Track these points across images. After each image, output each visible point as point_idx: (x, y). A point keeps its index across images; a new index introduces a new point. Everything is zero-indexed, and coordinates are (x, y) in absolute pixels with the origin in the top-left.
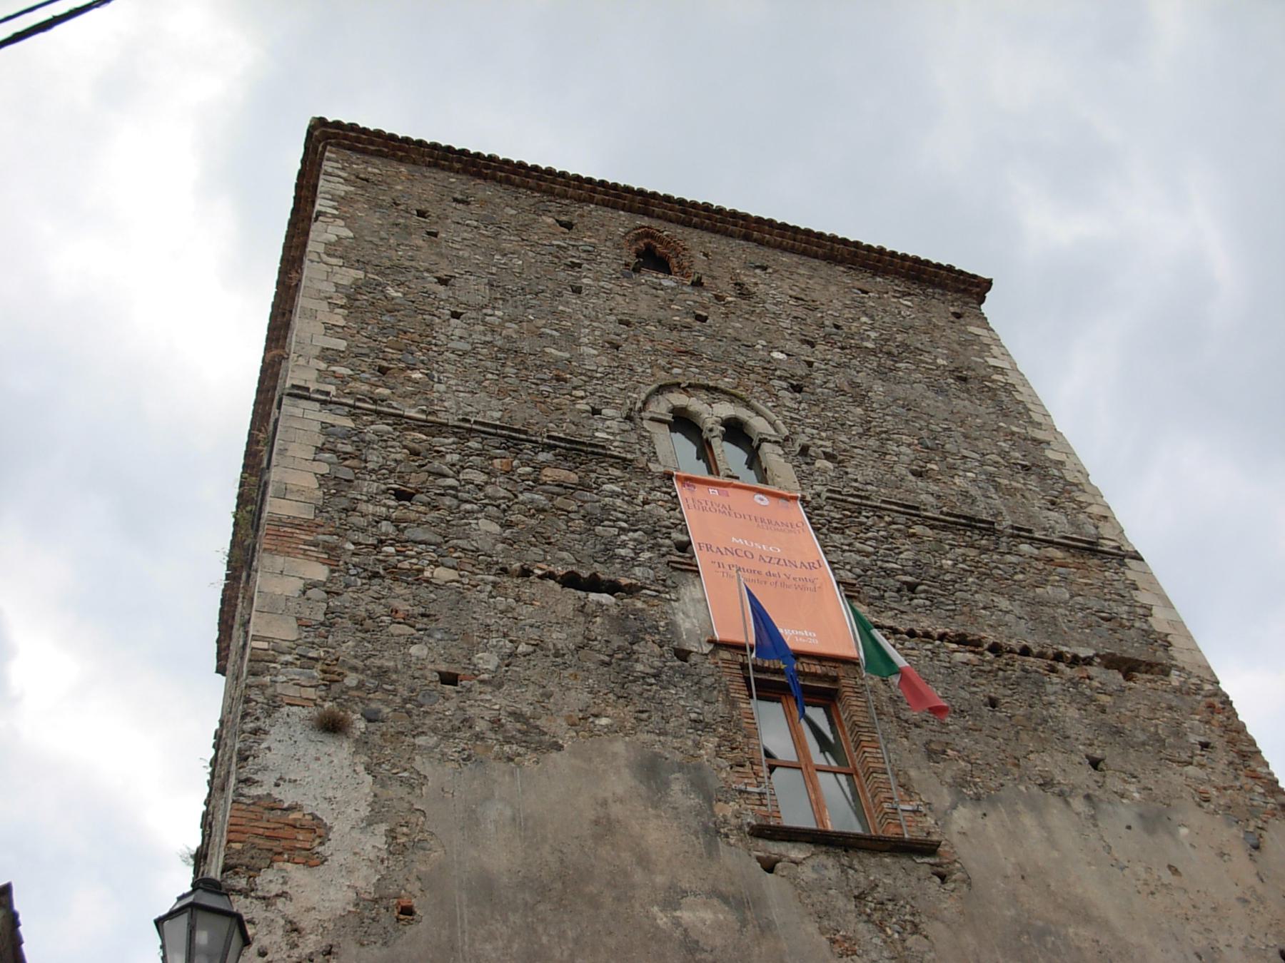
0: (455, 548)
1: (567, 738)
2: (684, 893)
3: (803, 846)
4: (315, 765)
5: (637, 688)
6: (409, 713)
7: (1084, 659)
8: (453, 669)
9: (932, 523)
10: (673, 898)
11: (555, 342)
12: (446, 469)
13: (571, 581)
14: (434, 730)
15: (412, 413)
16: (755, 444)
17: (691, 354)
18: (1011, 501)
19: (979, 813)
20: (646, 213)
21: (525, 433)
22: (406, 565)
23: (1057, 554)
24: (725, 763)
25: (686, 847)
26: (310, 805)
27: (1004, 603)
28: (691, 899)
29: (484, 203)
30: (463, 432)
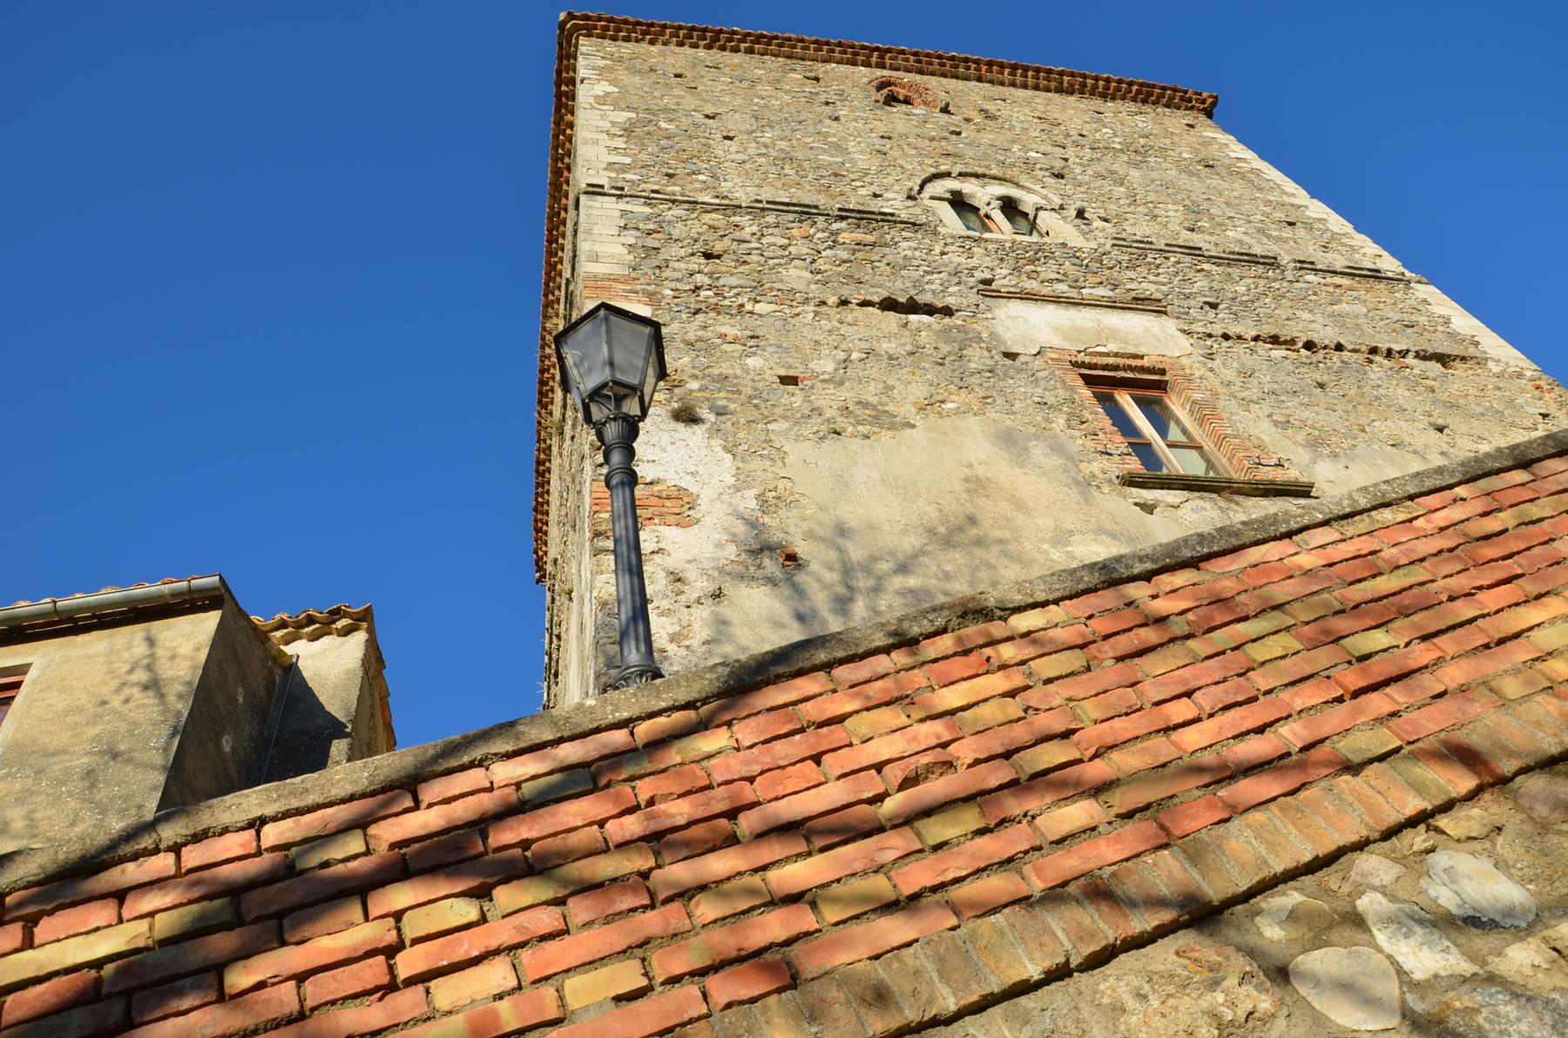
0: (771, 289)
1: (916, 420)
2: (1071, 533)
3: (1178, 492)
4: (670, 448)
5: (975, 380)
6: (756, 406)
7: (1400, 352)
9: (1216, 260)
11: (825, 151)
12: (748, 237)
13: (889, 305)
14: (785, 418)
15: (707, 199)
16: (1031, 217)
17: (956, 156)
18: (1286, 247)
19: (1341, 466)
21: (816, 207)
22: (727, 302)
23: (1345, 281)
24: (1077, 434)
25: (1061, 496)
28: (1078, 537)
29: (734, 67)
30: (758, 209)
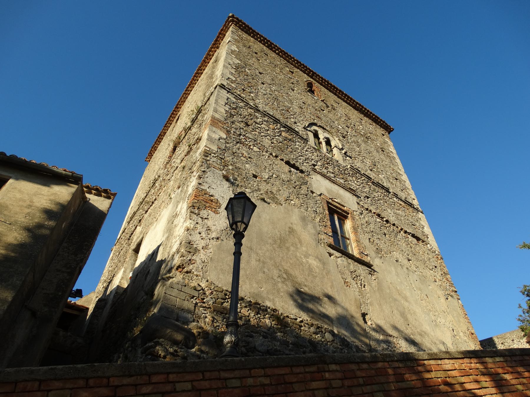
8: (257, 174)
10: (307, 256)
13: (288, 163)
20: (311, 77)
26: (217, 196)
27: (389, 211)
